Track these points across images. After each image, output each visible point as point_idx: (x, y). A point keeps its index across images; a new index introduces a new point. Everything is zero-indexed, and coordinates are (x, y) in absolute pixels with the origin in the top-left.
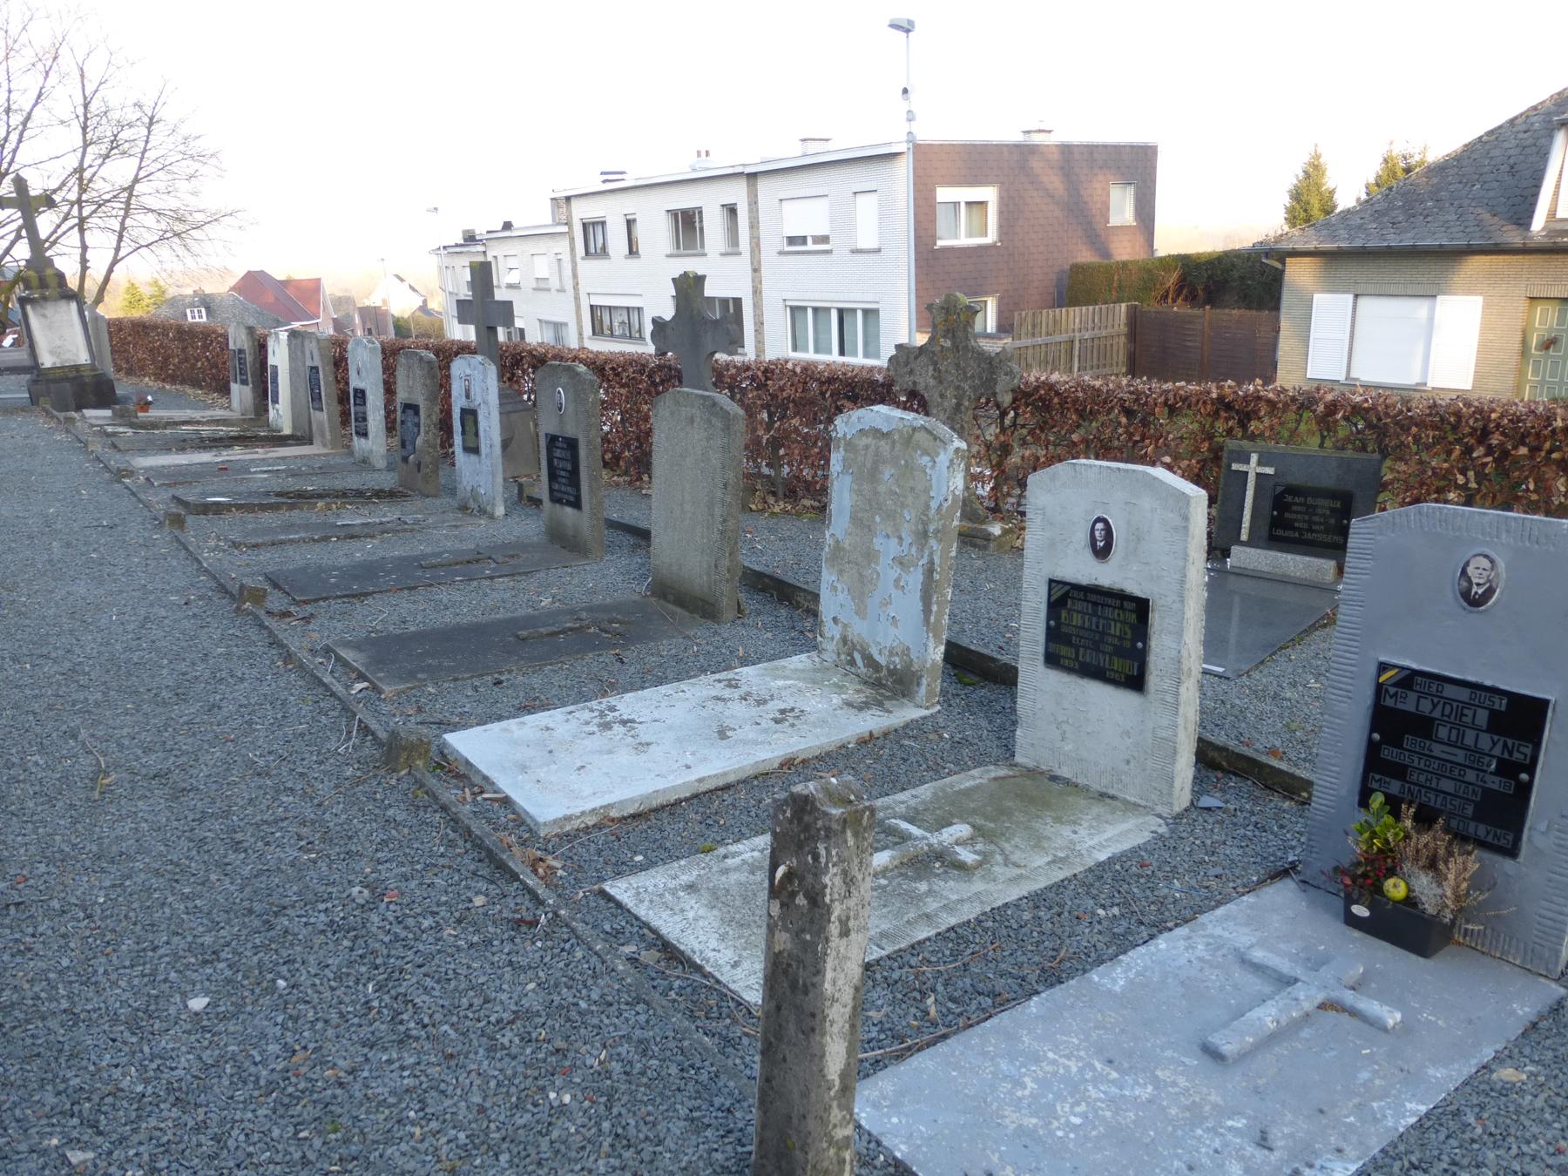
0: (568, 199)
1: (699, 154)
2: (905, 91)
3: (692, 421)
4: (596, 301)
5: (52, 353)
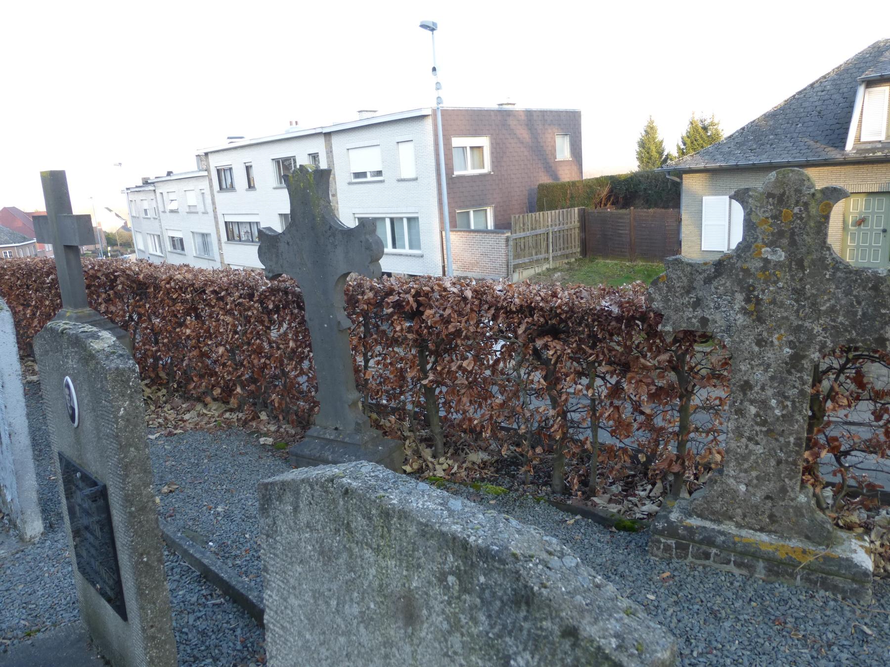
0: (206, 154)
1: (291, 123)
2: (434, 69)
3: (409, 612)
4: (229, 219)
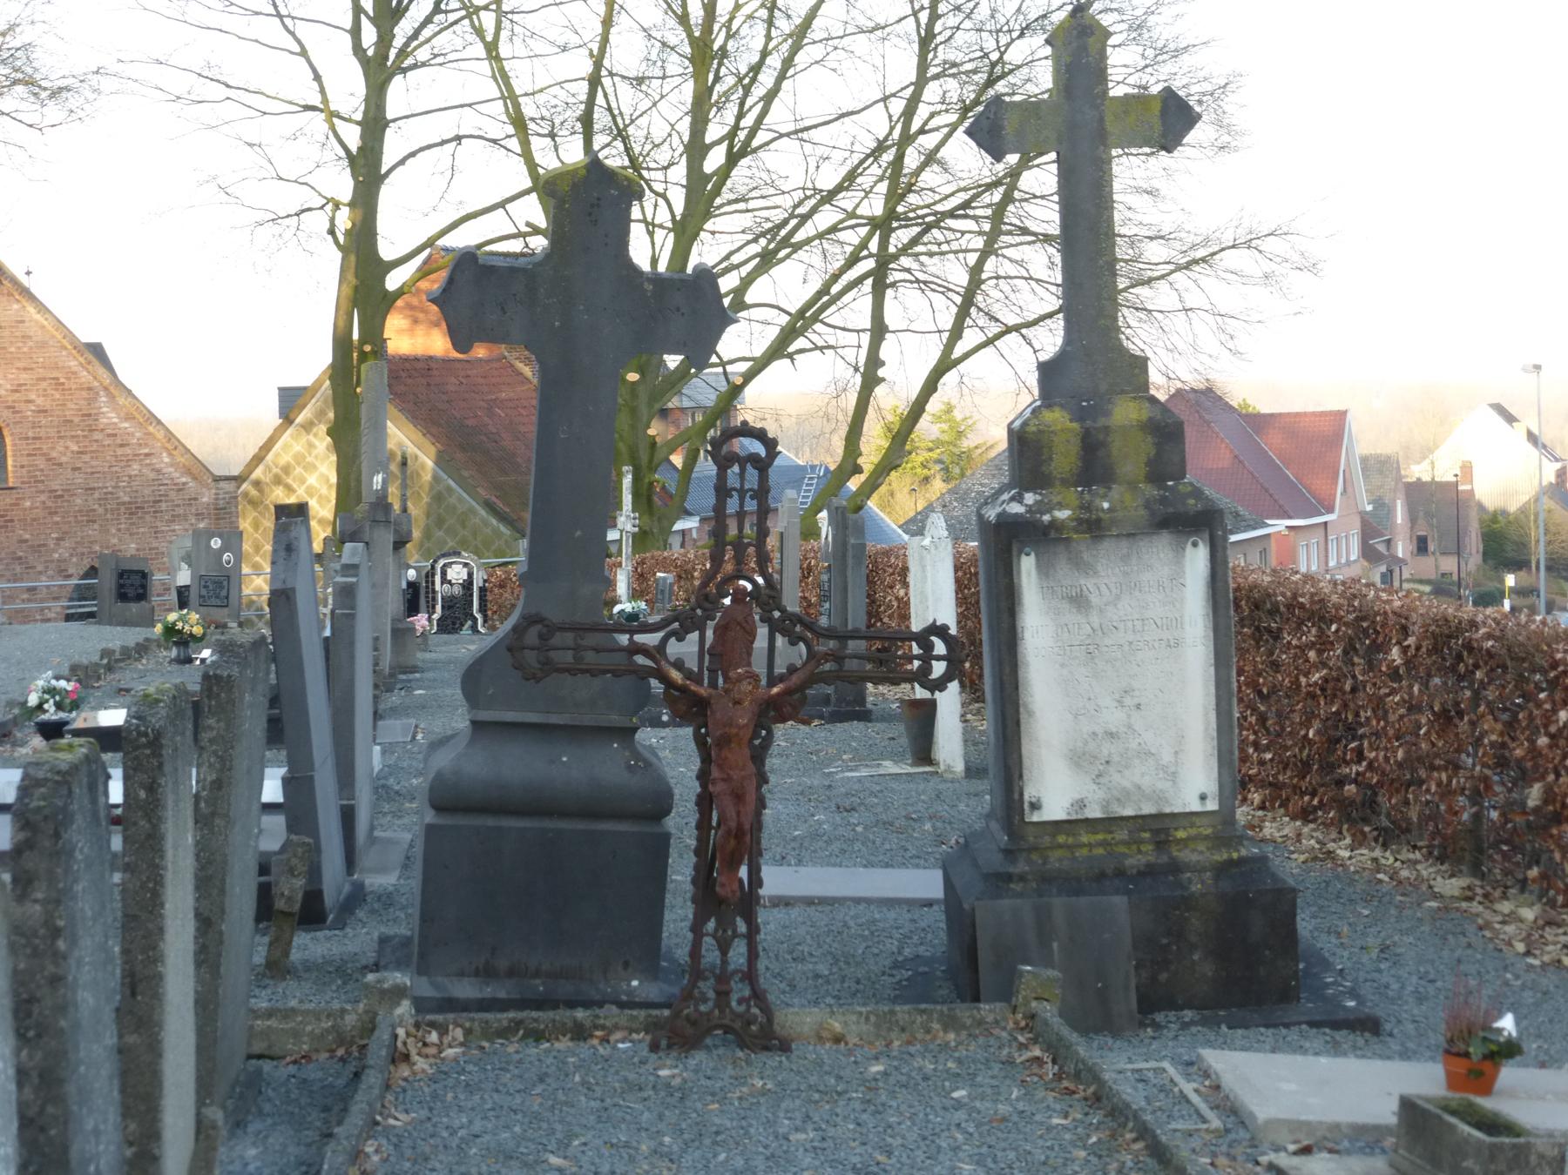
5: (1078, 759)
